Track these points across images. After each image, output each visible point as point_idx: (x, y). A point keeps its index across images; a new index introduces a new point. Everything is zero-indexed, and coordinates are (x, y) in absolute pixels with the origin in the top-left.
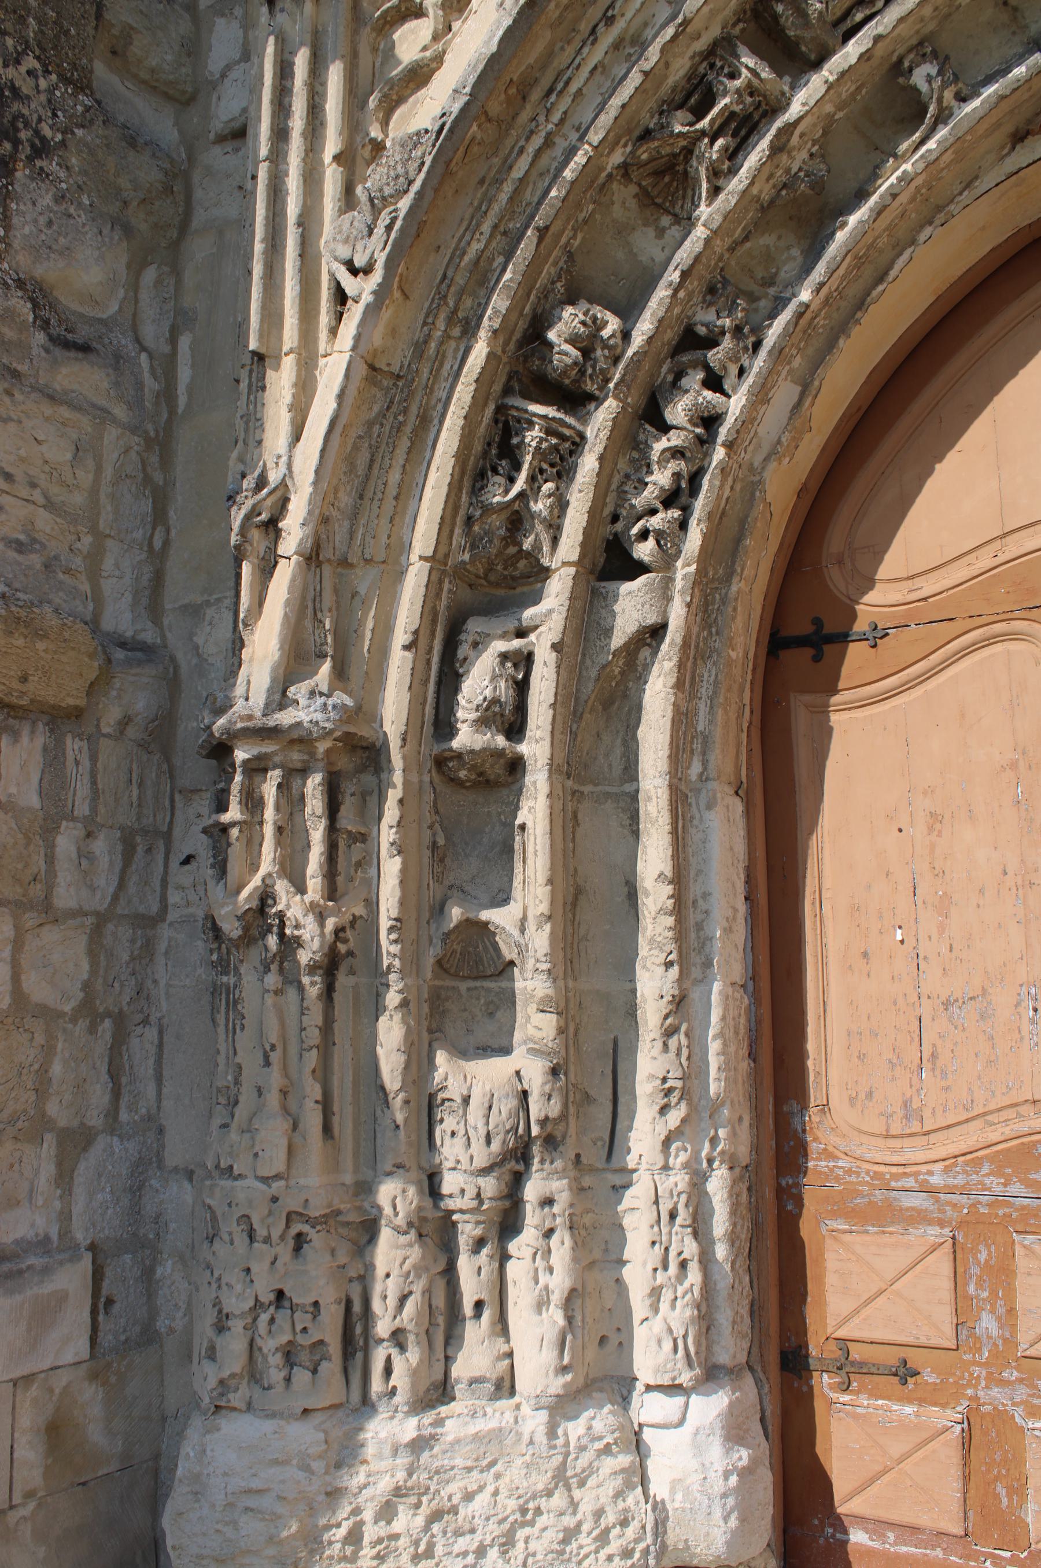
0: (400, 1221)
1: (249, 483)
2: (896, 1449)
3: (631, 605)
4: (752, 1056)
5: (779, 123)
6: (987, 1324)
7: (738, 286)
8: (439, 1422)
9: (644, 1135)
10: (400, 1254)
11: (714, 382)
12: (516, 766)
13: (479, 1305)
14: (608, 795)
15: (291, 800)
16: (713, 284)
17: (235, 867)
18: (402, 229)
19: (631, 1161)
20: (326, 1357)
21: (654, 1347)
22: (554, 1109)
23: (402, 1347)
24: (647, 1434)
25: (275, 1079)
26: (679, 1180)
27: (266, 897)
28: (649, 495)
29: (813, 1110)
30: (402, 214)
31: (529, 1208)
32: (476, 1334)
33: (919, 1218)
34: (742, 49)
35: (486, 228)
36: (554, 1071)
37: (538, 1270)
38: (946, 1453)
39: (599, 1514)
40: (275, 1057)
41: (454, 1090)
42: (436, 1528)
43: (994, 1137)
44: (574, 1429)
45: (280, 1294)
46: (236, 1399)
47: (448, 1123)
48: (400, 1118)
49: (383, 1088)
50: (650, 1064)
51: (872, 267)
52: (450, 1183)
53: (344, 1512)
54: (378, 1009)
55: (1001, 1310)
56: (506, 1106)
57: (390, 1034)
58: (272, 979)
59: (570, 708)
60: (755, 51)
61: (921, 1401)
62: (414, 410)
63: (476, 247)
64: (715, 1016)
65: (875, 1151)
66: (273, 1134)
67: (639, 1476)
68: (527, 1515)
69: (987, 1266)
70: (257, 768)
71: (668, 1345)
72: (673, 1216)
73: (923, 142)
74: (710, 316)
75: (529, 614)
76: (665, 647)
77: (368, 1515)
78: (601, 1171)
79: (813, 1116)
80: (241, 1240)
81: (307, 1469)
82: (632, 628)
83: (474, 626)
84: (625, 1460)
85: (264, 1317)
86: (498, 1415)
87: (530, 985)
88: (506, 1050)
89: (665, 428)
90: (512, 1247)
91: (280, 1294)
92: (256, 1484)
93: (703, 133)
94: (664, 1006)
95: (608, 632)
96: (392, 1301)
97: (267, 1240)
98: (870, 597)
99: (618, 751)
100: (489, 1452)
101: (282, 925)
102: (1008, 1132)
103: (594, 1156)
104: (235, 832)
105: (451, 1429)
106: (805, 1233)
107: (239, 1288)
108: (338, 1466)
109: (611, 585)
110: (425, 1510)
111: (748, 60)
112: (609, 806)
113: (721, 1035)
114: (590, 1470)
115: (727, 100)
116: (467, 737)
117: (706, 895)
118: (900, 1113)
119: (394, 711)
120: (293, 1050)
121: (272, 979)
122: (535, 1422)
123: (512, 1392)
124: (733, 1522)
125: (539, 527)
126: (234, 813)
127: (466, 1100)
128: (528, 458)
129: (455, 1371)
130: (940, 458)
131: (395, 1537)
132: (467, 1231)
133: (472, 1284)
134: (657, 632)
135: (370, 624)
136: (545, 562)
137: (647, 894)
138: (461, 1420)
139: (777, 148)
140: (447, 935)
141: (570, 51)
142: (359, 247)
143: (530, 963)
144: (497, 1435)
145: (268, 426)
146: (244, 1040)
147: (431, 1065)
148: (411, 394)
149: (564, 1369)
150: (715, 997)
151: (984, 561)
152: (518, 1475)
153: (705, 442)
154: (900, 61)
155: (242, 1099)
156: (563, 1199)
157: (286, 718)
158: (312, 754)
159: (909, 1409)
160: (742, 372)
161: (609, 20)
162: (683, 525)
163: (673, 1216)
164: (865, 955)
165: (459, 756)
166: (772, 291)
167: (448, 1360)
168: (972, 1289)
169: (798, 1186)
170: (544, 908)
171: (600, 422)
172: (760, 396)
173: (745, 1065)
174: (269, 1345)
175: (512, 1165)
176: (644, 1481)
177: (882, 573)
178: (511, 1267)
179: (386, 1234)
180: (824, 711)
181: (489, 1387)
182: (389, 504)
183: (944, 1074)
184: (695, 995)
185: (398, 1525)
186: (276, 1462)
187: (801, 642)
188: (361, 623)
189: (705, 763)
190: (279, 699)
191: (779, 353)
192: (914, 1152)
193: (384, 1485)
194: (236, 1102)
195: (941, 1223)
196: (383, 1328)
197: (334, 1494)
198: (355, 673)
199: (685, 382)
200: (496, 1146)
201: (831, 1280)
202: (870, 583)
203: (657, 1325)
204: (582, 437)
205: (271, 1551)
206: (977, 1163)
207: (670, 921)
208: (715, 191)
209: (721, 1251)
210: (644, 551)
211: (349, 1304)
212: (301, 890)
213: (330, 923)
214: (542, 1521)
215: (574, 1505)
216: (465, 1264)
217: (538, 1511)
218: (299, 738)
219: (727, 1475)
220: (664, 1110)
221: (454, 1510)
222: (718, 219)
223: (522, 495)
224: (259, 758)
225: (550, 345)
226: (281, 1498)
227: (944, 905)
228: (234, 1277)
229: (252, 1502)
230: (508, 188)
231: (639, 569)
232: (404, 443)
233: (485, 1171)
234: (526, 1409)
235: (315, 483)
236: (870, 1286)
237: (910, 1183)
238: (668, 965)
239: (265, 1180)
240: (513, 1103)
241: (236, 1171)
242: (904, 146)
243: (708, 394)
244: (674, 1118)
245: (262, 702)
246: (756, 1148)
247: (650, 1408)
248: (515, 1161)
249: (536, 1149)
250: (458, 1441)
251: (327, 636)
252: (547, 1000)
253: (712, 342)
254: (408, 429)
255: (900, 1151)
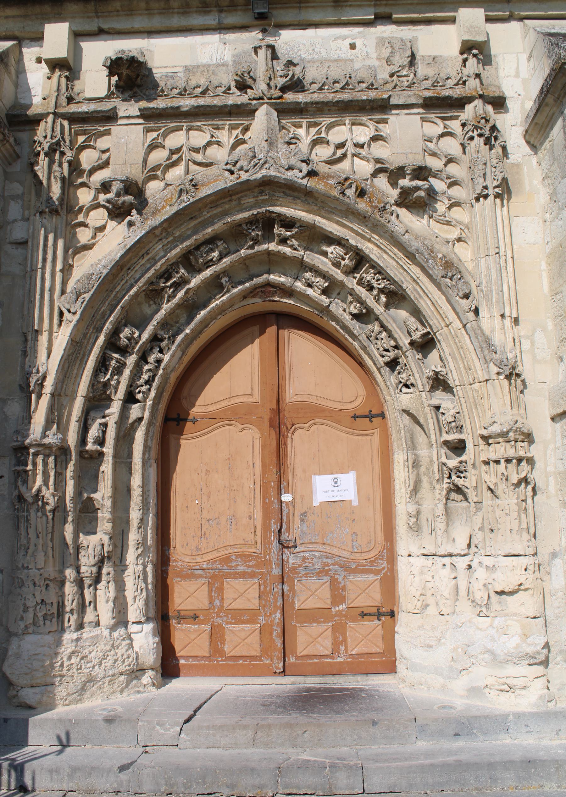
0: (72, 580)
1: (34, 371)
2: (193, 637)
3: (135, 411)
4: (157, 535)
5: (187, 287)
6: (217, 602)
7: (170, 326)
8: (82, 634)
9: (131, 555)
10: (72, 589)
11: (161, 351)
12: (101, 454)
13: (90, 603)
14: (123, 462)
15: (45, 464)
16: (164, 324)
17: (30, 482)
18: (86, 305)
19: (127, 563)
20: (53, 617)
21: (134, 611)
22: (111, 549)
23: (73, 615)
24: (132, 635)
25: (41, 541)
26: (140, 567)
27: (39, 491)
28: (142, 381)
29: (172, 549)
30: (87, 299)
31: (103, 576)
32: (89, 610)
33: (200, 576)
34: (181, 266)
35: (107, 304)
36: (110, 539)
37: (105, 593)
38: (205, 636)
39: (123, 655)
40: (40, 535)
41: (85, 544)
42: (82, 661)
43: (220, 555)
44: (115, 634)
45: (43, 600)
46: (30, 630)
47: (83, 553)
48: (71, 551)
49: (67, 544)
50: (133, 537)
51: (205, 323)
52: (83, 569)
53: (59, 658)
54: (65, 521)
55: (220, 599)
56: (99, 548)
57: (69, 529)
58: (40, 514)
59: (117, 439)
60: (185, 268)
61: (199, 624)
62: (82, 353)
63: (103, 308)
64: (150, 524)
65: (188, 559)
66: (41, 557)
67: (131, 646)
68: (105, 657)
69: (217, 588)
70: (36, 455)
71: (138, 611)
72: (139, 577)
73: (222, 296)
74: (162, 333)
75: (107, 412)
76: (143, 423)
77: (65, 659)
78: (120, 566)
79: (171, 550)
80: (31, 586)
81: (50, 647)
82: (135, 418)
83: (92, 414)
84: (128, 642)
85: (38, 607)
86: (96, 631)
87: (105, 515)
88: (95, 533)
89: (147, 363)
90: (98, 587)
91: (43, 600)
92: (37, 652)
93: (168, 287)
94: (138, 521)
95: (128, 418)
96: (70, 602)
97: (40, 586)
98: (194, 409)
99: (126, 450)
100: (95, 640)
101: (43, 498)
102: (223, 553)
103: (118, 562)
104: (30, 473)
105: (85, 636)
106: (168, 582)
107: (31, 599)
108: (57, 647)
109: (129, 405)
110: (80, 657)
111: (182, 271)
112: (123, 465)
113: (151, 529)
114: (120, 645)
115: (175, 279)
116: (90, 446)
117: (148, 491)
118: (195, 549)
119: (72, 439)
120: (45, 534)
121: (40, 514)
122: (106, 632)
123: (99, 626)
124: (155, 656)
125: (112, 388)
126: (30, 467)
127: (88, 546)
128: (111, 369)
129: (84, 621)
130: (215, 374)
131: (72, 664)
132: (87, 582)
133: (88, 597)
134: (140, 419)
135: (66, 414)
136: (113, 397)
137: (134, 490)
138: (88, 633)
139: (186, 293)
140: (83, 501)
141: (136, 259)
142: (73, 306)
143: (105, 509)
144: (97, 636)
145: (39, 352)
146: (31, 531)
147: (78, 537)
148: (81, 349)
149: (114, 618)
150: (150, 518)
151: (225, 404)
152: (102, 646)
153: (157, 367)
154: (219, 275)
155: (31, 547)
156: (112, 573)
157: (47, 441)
158: (52, 451)
159: (196, 626)
160: (169, 349)
161: (148, 254)
162: (149, 390)
163: (139, 577)
164: (187, 507)
165: (87, 451)
166: (177, 325)
167: (83, 618)
168: (213, 594)
169: (167, 570)
170: (110, 494)
171: (131, 360)
172: (173, 356)
173: (155, 536)
174: (40, 615)
175: (99, 564)
176: (132, 647)
177: (197, 403)
178: (98, 592)
179: (68, 584)
180: (179, 440)
181: (94, 624)
182: (73, 379)
183: (207, 539)
184: (145, 518)
185: (73, 661)
186: (42, 646)
187: (174, 420)
188: (64, 413)
189: (149, 455)
190: (44, 436)
191: (179, 346)
192: (199, 559)
193: (69, 651)
194: (28, 548)
195: (206, 578)
196: (68, 609)
197: (57, 654)
198: (61, 427)
199: (154, 350)
200: (96, 559)
201: (176, 594)
202: (193, 405)
203: (135, 606)
204: (125, 363)
205: (42, 669)
206: (215, 561)
207: (141, 498)
208: (168, 301)
209: (150, 587)
210: (139, 396)
211: (59, 603)
212: (49, 489)
213: (56, 498)
214: (109, 658)
215: (116, 653)
216: (86, 592)
217: (108, 656)
218: (48, 447)
219: (154, 644)
220: (137, 549)
221: (87, 656)
222: (169, 310)
223: (109, 379)
224: (37, 451)
225: (120, 338)
226: (44, 655)
227: (209, 494)
228: (30, 597)
229: (36, 657)
230: (114, 293)
231: (138, 401)
232: (78, 362)
233: (93, 566)
234: (103, 629)
235: (56, 374)
236: (186, 595)
237: (198, 567)
238: (140, 510)
239: (39, 569)
240: (100, 547)
241: (30, 567)
242: (218, 297)
243: (159, 354)
244: (140, 551)
245: (39, 436)
246: (157, 560)
247: (133, 628)
248: (100, 564)
249: (106, 559)
250: (87, 638)
251: (56, 417)
252: (109, 519)
253: (162, 340)
254: (80, 358)
255: (195, 559)
